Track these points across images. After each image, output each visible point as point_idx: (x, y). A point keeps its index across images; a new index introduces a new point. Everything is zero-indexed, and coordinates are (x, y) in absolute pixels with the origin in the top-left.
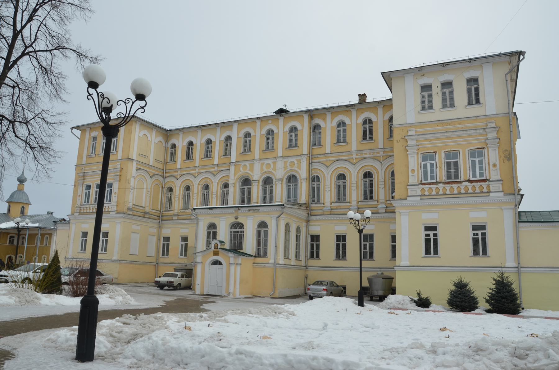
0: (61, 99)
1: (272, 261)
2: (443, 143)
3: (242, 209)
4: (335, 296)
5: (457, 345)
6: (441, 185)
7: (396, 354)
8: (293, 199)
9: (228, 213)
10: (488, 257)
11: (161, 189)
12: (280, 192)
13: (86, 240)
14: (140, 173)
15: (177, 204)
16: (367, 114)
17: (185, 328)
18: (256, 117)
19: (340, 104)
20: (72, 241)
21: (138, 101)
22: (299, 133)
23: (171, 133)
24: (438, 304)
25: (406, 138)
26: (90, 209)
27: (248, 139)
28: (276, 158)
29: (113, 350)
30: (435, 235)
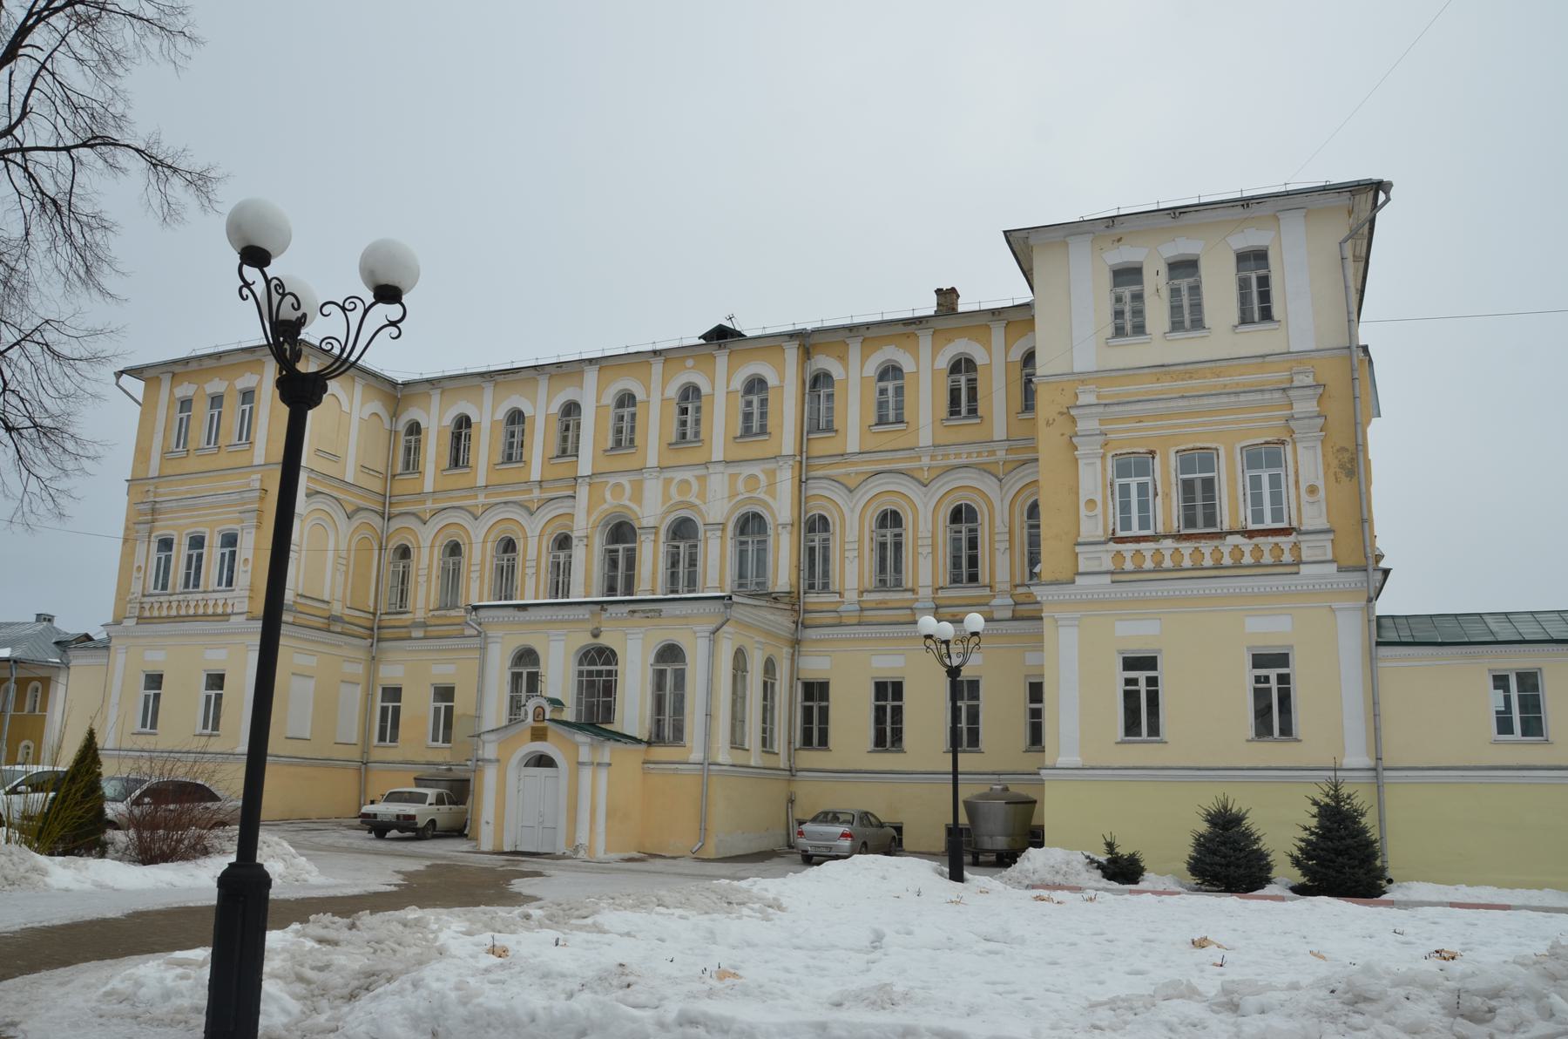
0: (103, 292)
1: (696, 756)
2: (1175, 426)
3: (611, 608)
5: (1294, 987)
6: (1168, 543)
7: (1130, 1017)
8: (755, 580)
9: (573, 621)
12: (717, 561)
13: (157, 697)
15: (424, 594)
16: (961, 346)
17: (492, 951)
18: (650, 348)
20: (114, 699)
21: (380, 306)
22: (771, 396)
23: (406, 391)
25: (1073, 412)
26: (169, 607)
27: (626, 412)
28: (706, 465)
29: (309, 1022)
30: (1152, 681)
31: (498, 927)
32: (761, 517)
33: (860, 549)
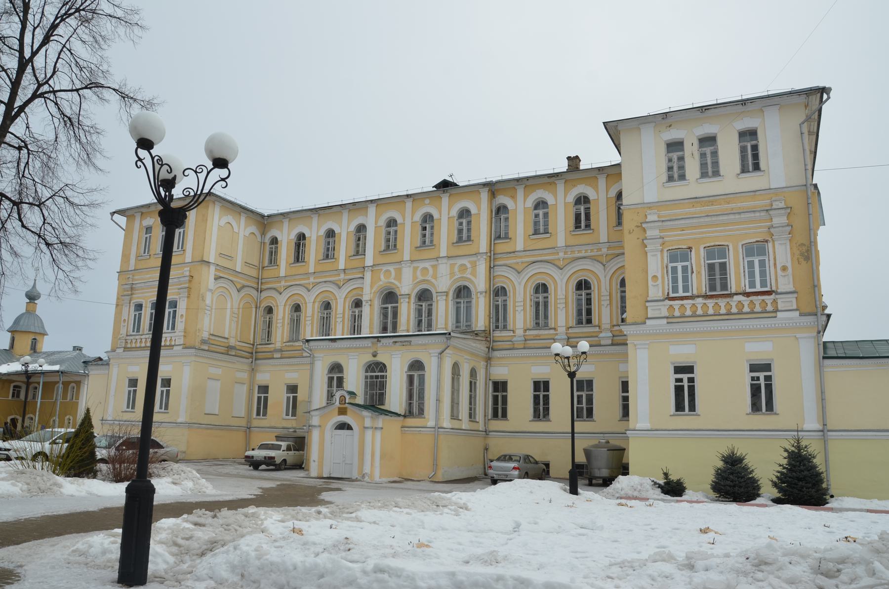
0: (93, 165)
1: (431, 423)
3: (383, 340)
4: (534, 477)
6: (700, 300)
7: (630, 571)
10: (776, 414)
11: (254, 310)
12: (443, 313)
14: (221, 283)
17: (294, 531)
18: (405, 193)
19: (539, 173)
20: (112, 392)
21: (216, 170)
22: (473, 219)
23: (270, 220)
25: (644, 225)
26: (141, 342)
27: (392, 229)
28: (437, 259)
30: (691, 380)
33: (525, 305)
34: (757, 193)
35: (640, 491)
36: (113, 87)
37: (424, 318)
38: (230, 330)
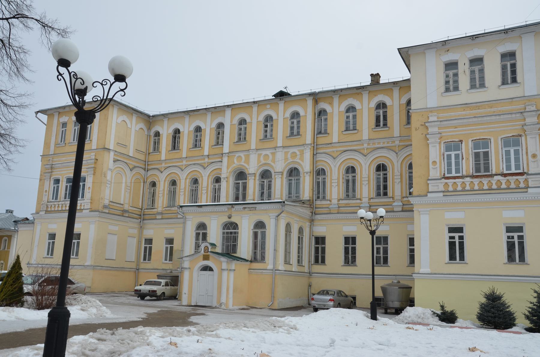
0: (23, 77)
1: (270, 267)
3: (236, 207)
4: (344, 307)
6: (468, 179)
8: (295, 195)
10: (527, 264)
11: (142, 184)
13: (53, 243)
14: (118, 164)
15: (162, 201)
16: (381, 98)
18: (252, 100)
19: (350, 86)
20: (36, 243)
21: (117, 83)
22: (302, 119)
23: (154, 119)
24: (465, 319)
25: (427, 124)
26: (58, 207)
27: (243, 127)
28: (275, 148)
30: (461, 238)
31: (175, 334)
32: (297, 169)
34: (514, 100)
35: (423, 318)
36: (36, 18)
37: (266, 191)
38: (124, 198)
